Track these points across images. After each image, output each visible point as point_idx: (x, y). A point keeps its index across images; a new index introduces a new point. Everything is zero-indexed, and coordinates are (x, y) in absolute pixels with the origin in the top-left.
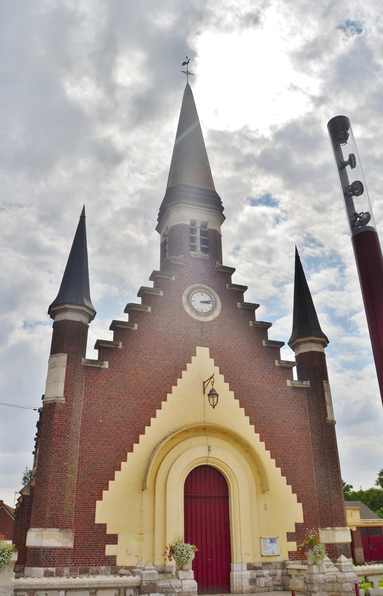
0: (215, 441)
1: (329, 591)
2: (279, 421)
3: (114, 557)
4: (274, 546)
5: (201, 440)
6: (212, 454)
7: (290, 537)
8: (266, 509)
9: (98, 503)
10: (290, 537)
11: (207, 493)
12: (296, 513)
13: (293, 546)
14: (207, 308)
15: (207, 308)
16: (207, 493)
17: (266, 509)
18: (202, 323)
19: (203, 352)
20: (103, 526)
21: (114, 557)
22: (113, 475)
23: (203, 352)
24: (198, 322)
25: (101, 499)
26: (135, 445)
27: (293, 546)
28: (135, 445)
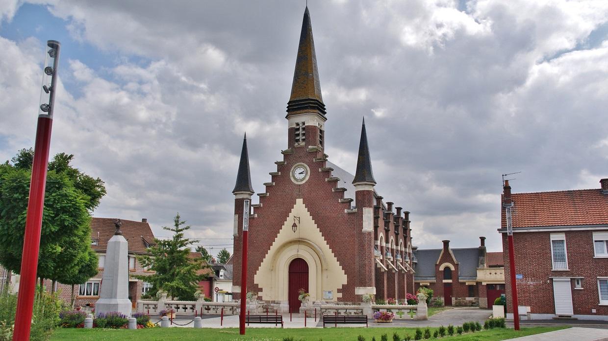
0: (302, 247)
1: (74, 109)
2: (338, 233)
3: (262, 297)
4: (330, 295)
5: (295, 247)
6: (299, 253)
7: (339, 291)
8: (327, 277)
9: (290, 214)
10: (339, 291)
11: (298, 272)
12: (343, 279)
13: (340, 295)
14: (302, 176)
15: (302, 176)
16: (298, 272)
17: (327, 277)
18: (300, 185)
19: (300, 201)
20: (257, 285)
21: (262, 297)
22: (265, 256)
23: (300, 201)
24: (297, 185)
25: (277, 237)
26: (269, 251)
27: (340, 295)
28: (269, 251)
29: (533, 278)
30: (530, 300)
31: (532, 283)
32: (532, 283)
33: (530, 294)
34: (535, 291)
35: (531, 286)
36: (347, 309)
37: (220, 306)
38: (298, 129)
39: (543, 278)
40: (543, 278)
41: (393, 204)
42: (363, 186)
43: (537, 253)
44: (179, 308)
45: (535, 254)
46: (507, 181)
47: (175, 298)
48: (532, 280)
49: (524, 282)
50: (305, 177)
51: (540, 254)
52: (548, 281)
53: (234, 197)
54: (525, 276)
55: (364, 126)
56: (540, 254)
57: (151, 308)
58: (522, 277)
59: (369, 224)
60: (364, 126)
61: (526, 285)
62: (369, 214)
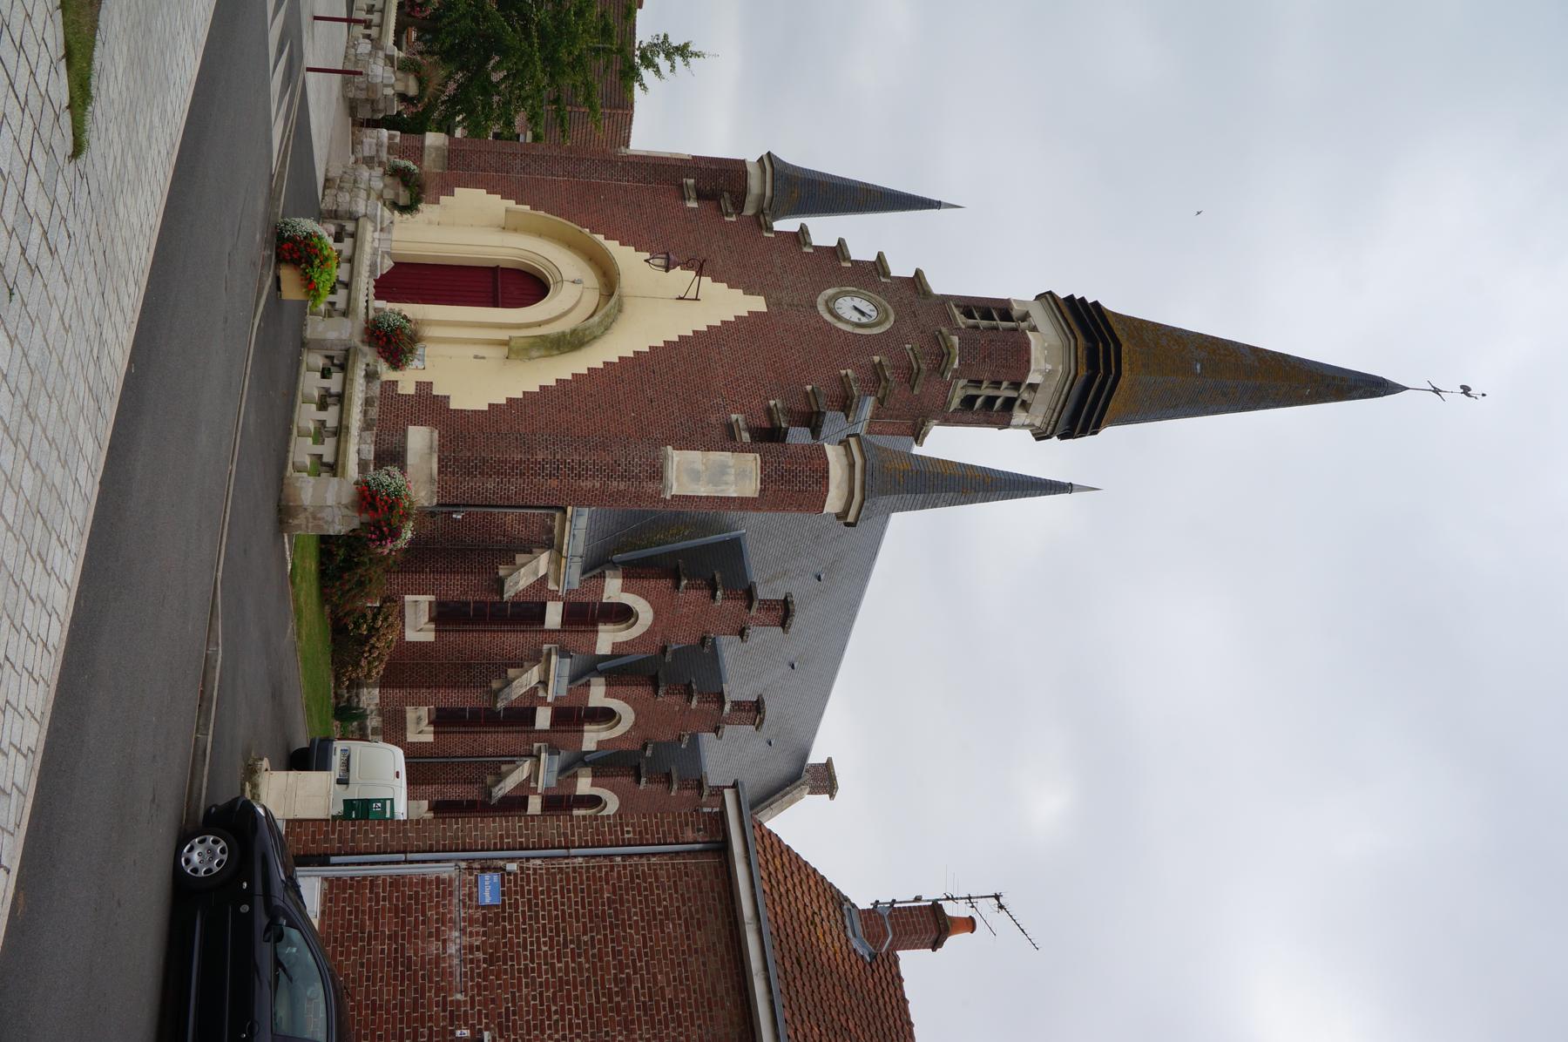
14: (855, 317)
29: (480, 955)
30: (355, 940)
31: (452, 949)
32: (452, 949)
33: (393, 937)
34: (408, 963)
35: (434, 947)
36: (347, 285)
37: (382, 18)
38: (1016, 385)
39: (485, 1004)
40: (485, 1004)
41: (832, 796)
42: (844, 461)
43: (629, 982)
44: (323, 406)
45: (621, 967)
46: (970, 924)
47: (370, 437)
48: (471, 949)
49: (457, 912)
50: (847, 322)
51: (624, 994)
52: (467, 1033)
53: (751, 157)
54: (492, 917)
55: (1065, 488)
56: (624, 994)
57: (318, 449)
58: (488, 901)
59: (695, 476)
60: (1065, 488)
61: (442, 920)
62: (737, 475)
